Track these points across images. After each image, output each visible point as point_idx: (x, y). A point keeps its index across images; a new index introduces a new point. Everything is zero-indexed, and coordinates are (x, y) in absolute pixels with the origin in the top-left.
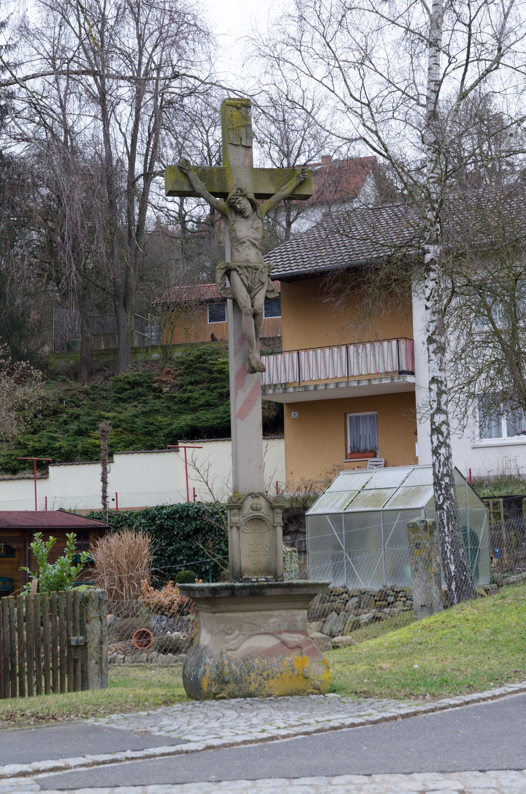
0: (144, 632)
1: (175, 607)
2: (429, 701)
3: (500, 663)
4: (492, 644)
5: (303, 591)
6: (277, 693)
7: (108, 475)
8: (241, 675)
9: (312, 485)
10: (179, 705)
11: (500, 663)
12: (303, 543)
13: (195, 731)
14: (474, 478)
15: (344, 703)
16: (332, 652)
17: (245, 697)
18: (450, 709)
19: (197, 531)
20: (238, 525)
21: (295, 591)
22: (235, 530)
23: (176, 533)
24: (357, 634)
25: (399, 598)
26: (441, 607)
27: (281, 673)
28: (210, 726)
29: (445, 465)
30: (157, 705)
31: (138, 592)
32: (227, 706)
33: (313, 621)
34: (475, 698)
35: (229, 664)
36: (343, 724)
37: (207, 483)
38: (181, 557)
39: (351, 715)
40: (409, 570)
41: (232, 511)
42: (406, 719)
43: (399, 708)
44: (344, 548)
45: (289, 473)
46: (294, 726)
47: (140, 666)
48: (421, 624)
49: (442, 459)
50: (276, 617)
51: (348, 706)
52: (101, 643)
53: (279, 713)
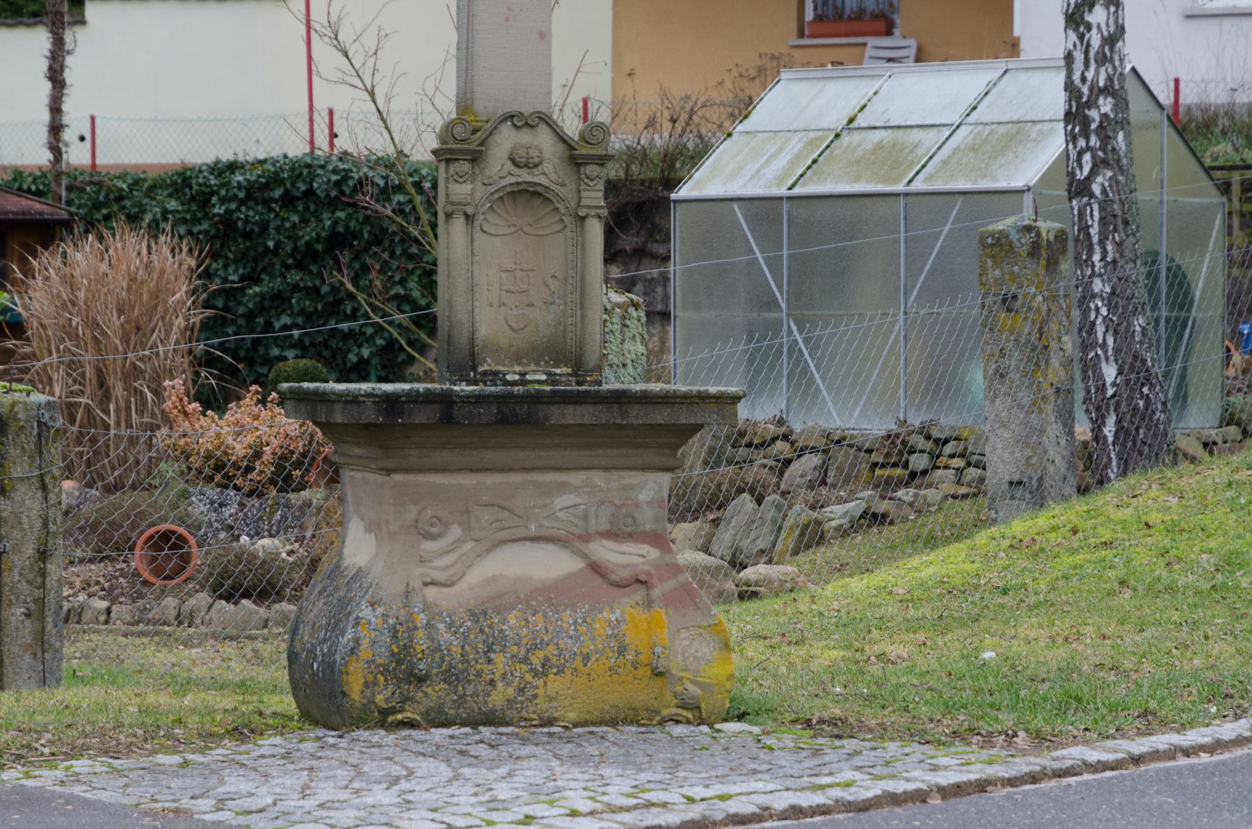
0: (166, 536)
1: (264, 468)
2: (1024, 753)
3: (1239, 652)
4: (1217, 597)
5: (661, 416)
6: (572, 716)
7: (69, 60)
8: (464, 660)
9: (692, 113)
10: (278, 740)
11: (1239, 652)
12: (659, 290)
13: (324, 813)
14: (1189, 108)
15: (771, 749)
16: (737, 608)
17: (474, 724)
18: (1087, 777)
19: (336, 240)
20: (470, 211)
21: (637, 416)
22: (459, 223)
23: (271, 244)
24: (813, 562)
25: (943, 460)
26: (1069, 489)
27: (586, 658)
28: (370, 800)
29: (1102, 60)
30: (209, 738)
31: (153, 415)
32: (420, 748)
33: (683, 519)
34: (1162, 747)
35: (429, 626)
36: (766, 809)
37: (372, 94)
38: (285, 320)
39: (789, 783)
40: (979, 375)
41: (453, 168)
42: (952, 801)
43: (935, 768)
44: (784, 305)
45: (624, 72)
46: (622, 809)
47: (157, 633)
48: (1009, 533)
49: (1095, 40)
50: (577, 492)
51: (781, 758)
52: (43, 555)
53: (575, 772)
